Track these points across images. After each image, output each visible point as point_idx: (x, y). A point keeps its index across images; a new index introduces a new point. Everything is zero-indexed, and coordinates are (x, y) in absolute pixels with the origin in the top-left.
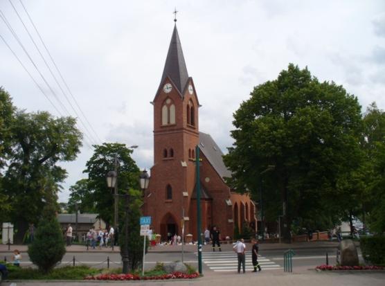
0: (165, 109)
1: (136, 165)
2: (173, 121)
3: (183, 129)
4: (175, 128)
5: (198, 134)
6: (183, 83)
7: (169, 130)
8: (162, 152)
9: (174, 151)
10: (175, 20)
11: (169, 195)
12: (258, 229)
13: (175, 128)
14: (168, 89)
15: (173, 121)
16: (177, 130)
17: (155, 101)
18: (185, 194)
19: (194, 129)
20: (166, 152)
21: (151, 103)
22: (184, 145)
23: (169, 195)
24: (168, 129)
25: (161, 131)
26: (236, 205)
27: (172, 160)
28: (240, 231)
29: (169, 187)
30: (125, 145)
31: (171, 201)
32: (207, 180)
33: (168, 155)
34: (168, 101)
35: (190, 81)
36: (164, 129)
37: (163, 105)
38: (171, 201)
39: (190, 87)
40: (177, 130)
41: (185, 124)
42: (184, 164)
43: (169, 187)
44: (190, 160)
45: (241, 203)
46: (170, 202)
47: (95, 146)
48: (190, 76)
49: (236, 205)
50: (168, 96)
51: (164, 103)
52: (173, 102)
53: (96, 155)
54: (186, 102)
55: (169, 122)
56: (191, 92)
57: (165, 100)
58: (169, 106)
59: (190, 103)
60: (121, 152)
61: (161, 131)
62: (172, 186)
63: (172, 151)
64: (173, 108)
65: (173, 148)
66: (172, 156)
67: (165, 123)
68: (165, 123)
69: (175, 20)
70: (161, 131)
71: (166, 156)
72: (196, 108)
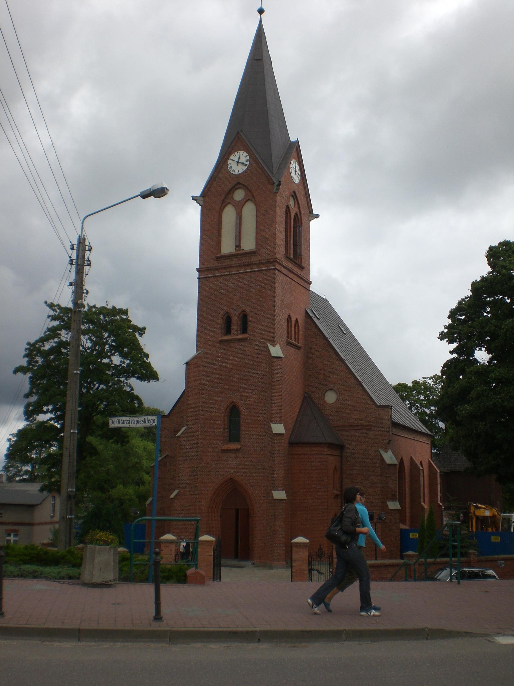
0: (229, 215)
1: (149, 364)
2: (249, 244)
3: (275, 261)
4: (255, 259)
5: (309, 291)
6: (277, 152)
7: (241, 266)
8: (220, 321)
9: (250, 318)
10: (261, 11)
11: (234, 434)
12: (511, 526)
13: (255, 259)
14: (239, 163)
15: (249, 244)
16: (260, 264)
17: (204, 194)
18: (278, 428)
19: (302, 268)
20: (228, 321)
21: (194, 198)
22: (278, 302)
23: (234, 434)
24: (234, 261)
25: (216, 269)
26: (401, 462)
27: (245, 339)
28: (426, 522)
29: (234, 411)
30: (126, 312)
31: (239, 447)
32: (331, 398)
33: (235, 327)
34: (239, 195)
35: (294, 150)
36: (227, 262)
37: (224, 204)
38: (237, 446)
39: (294, 164)
40: (260, 264)
41: (280, 252)
42: (276, 351)
43: (234, 411)
44: (289, 344)
45: (412, 461)
46: (237, 450)
47: (51, 306)
48: (293, 139)
49: (401, 462)
50: (238, 182)
51: (226, 198)
52: (250, 197)
53: (53, 333)
54: (283, 199)
55: (238, 247)
56: (296, 179)
57: (231, 191)
58: (239, 207)
59: (292, 203)
60: (117, 330)
61: (214, 264)
62: (243, 409)
63: (244, 318)
64: (249, 211)
65: (248, 310)
66: (244, 330)
67: (227, 247)
68: (227, 247)
69: (261, 11)
70: (216, 269)
71: (228, 331)
72: (304, 219)
